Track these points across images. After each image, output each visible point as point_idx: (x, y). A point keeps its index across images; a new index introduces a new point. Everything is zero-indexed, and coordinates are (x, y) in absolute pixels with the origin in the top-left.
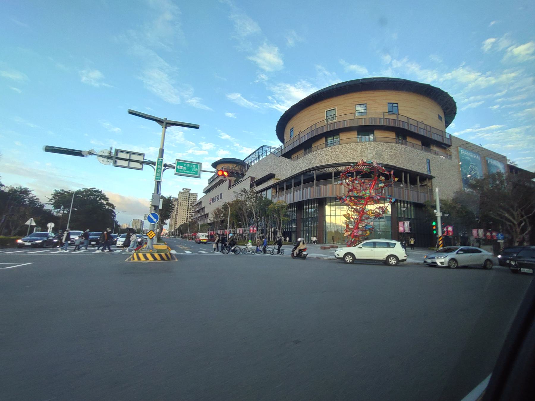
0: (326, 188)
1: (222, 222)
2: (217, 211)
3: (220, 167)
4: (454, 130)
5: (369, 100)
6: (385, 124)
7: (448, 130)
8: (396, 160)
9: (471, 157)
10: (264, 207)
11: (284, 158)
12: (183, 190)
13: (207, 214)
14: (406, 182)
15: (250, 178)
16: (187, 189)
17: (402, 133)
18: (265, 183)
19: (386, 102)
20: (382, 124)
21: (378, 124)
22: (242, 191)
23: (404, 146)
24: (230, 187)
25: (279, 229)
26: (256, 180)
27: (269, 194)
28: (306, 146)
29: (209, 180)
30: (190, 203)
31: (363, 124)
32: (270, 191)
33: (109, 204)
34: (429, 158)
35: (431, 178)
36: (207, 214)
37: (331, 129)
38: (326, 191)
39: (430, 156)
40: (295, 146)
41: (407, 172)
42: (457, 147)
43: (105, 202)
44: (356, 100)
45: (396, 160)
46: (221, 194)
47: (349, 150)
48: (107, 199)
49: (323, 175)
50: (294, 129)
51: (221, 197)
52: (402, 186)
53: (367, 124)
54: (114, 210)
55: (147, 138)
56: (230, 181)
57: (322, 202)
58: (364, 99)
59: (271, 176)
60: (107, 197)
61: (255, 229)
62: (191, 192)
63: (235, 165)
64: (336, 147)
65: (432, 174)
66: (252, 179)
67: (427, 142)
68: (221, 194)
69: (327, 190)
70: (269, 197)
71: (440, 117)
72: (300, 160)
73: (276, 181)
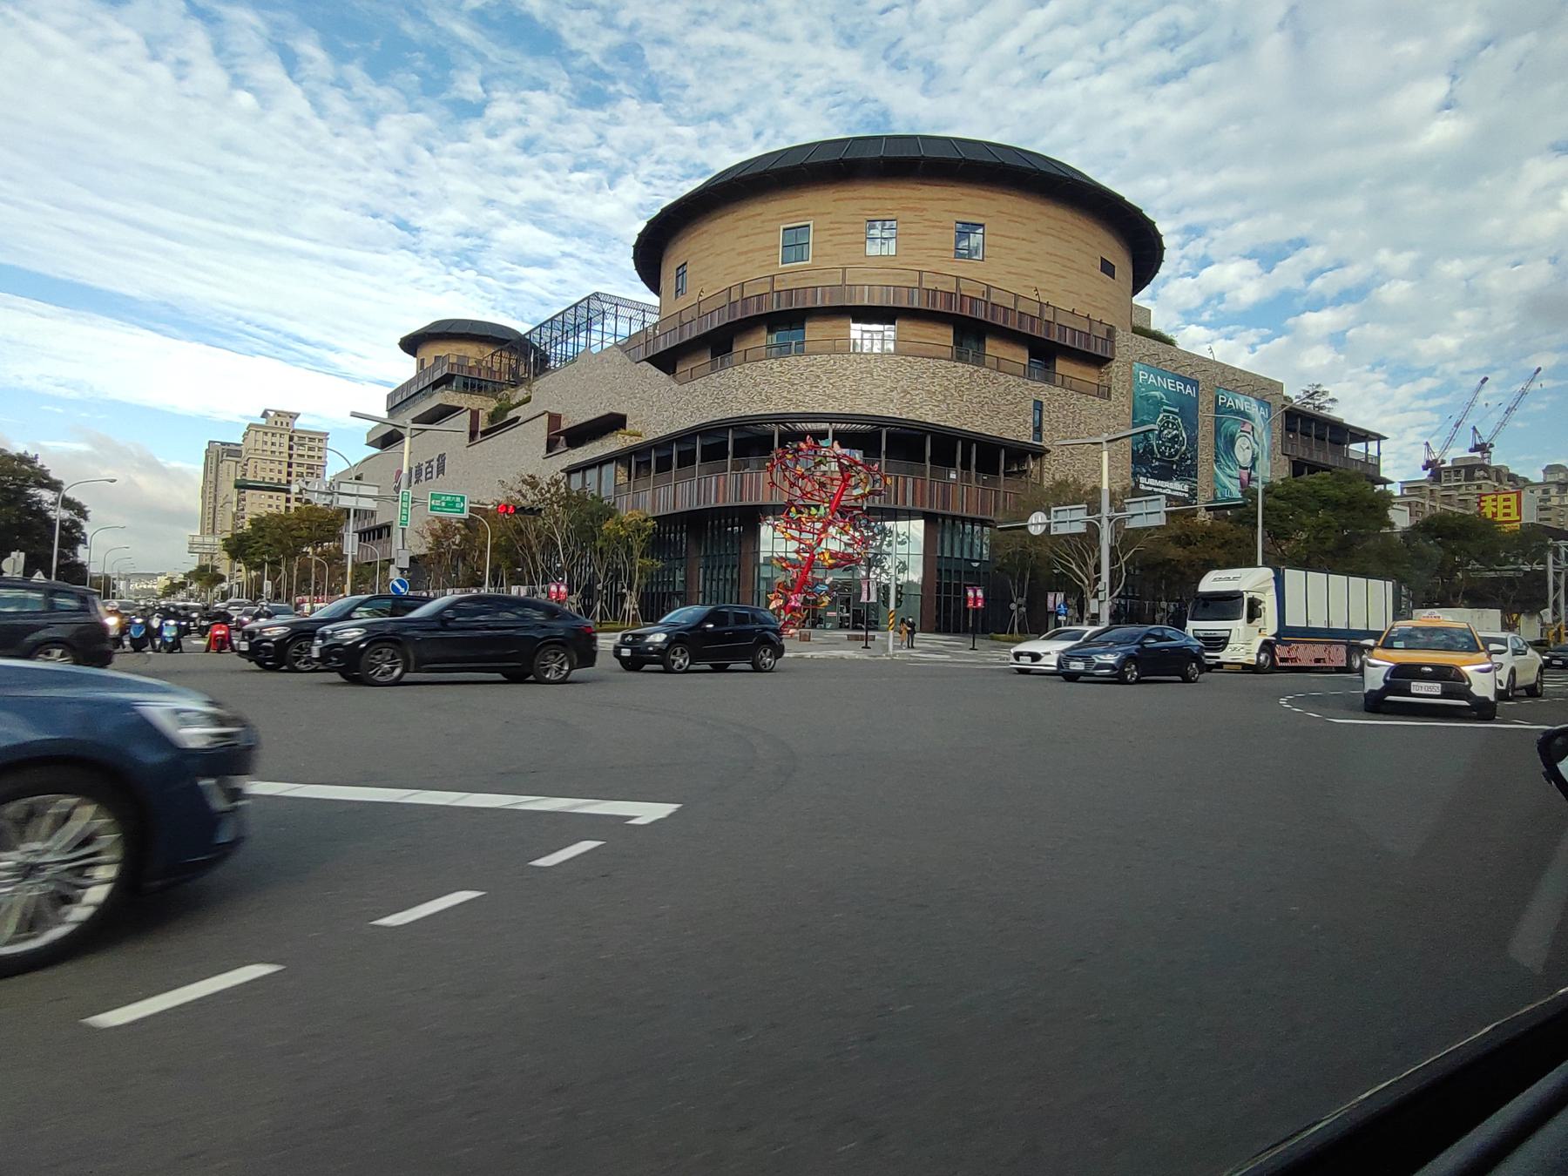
0: (758, 479)
1: (462, 555)
2: (437, 526)
3: (431, 352)
4: (1165, 302)
5: (904, 209)
6: (924, 307)
7: (1136, 300)
8: (944, 406)
9: (1166, 392)
10: (590, 518)
11: (655, 371)
12: (265, 414)
13: (388, 527)
14: (966, 465)
15: (545, 418)
16: (278, 414)
17: (971, 329)
18: (597, 443)
19: (950, 220)
20: (916, 305)
21: (904, 304)
22: (524, 481)
23: (970, 368)
24: (473, 435)
25: (630, 588)
26: (565, 425)
27: (610, 479)
28: (719, 342)
29: (390, 397)
30: (295, 469)
31: (866, 303)
32: (608, 470)
33: (68, 504)
34: (1042, 398)
35: (1039, 453)
36: (388, 527)
37: (783, 308)
38: (757, 486)
39: (1043, 391)
40: (687, 338)
41: (969, 439)
42: (1131, 364)
43: (47, 495)
44: (868, 204)
45: (944, 406)
46: (442, 457)
47: (825, 372)
48: (55, 486)
49: (751, 440)
50: (688, 268)
51: (441, 470)
52: (953, 476)
53: (876, 303)
54: (83, 522)
55: (221, 322)
56: (475, 415)
57: (751, 517)
58: (889, 204)
59: (614, 423)
60: (54, 475)
61: (563, 589)
62: (299, 424)
63: (489, 350)
64: (792, 360)
65: (1046, 443)
66: (554, 419)
67: (1044, 352)
68: (442, 457)
69: (757, 484)
70: (607, 490)
71: (1108, 268)
72: (698, 384)
73: (631, 441)
